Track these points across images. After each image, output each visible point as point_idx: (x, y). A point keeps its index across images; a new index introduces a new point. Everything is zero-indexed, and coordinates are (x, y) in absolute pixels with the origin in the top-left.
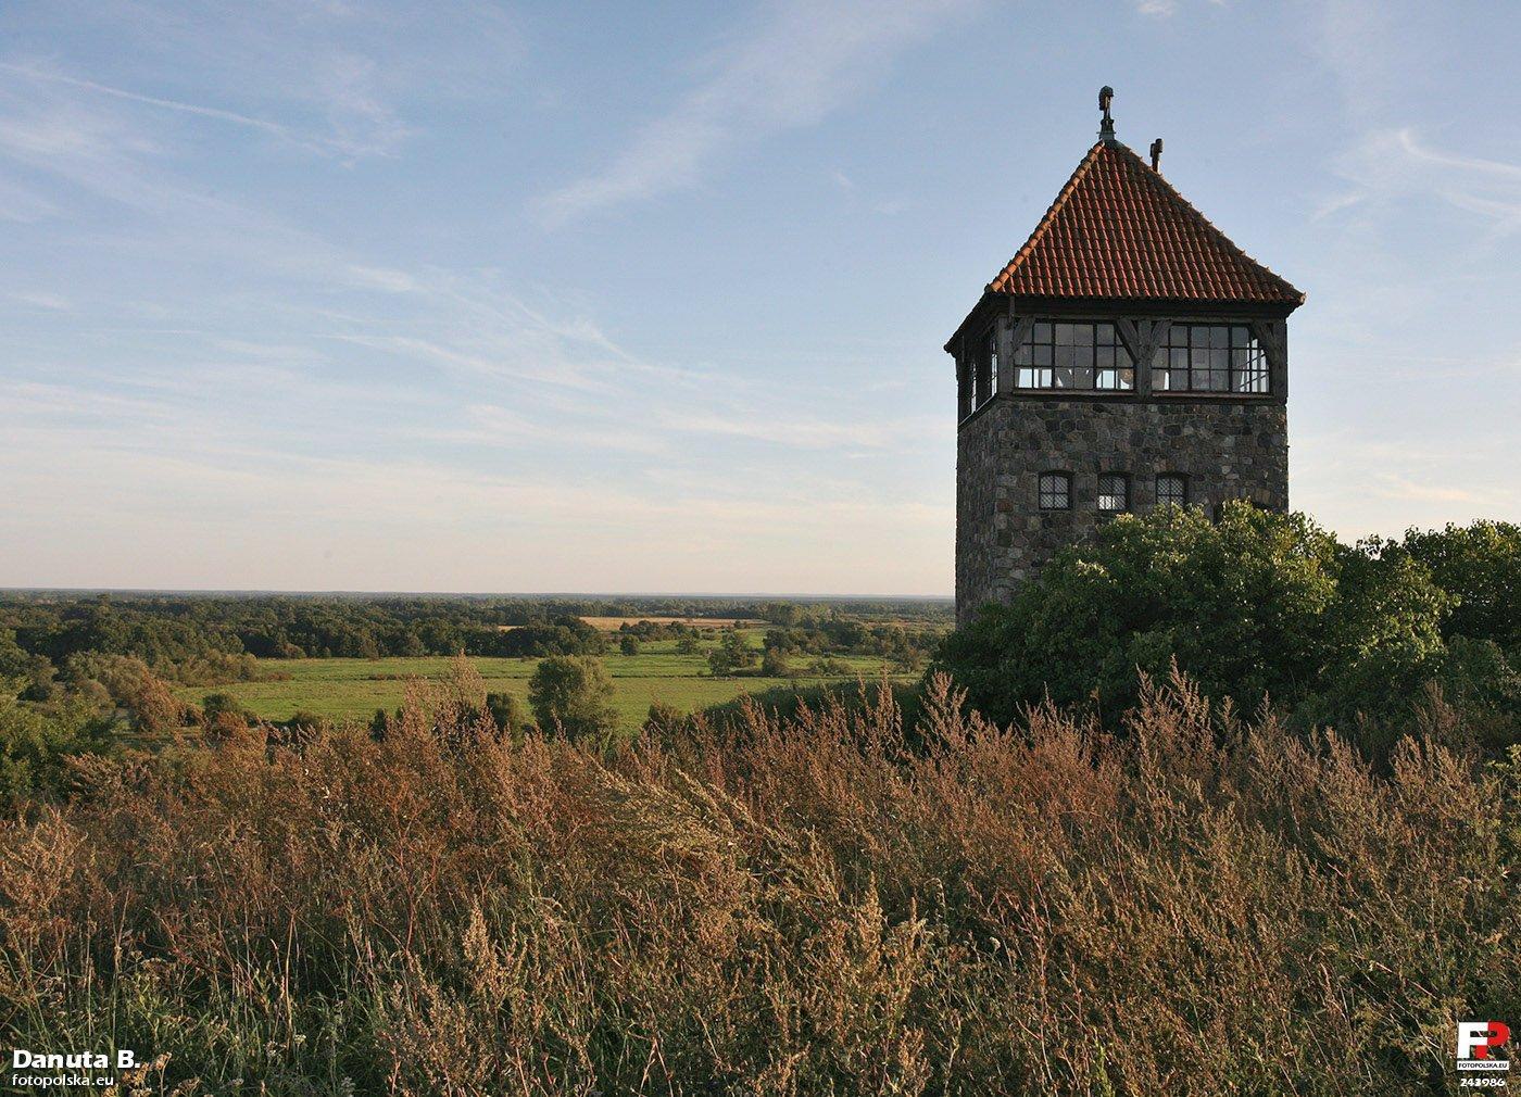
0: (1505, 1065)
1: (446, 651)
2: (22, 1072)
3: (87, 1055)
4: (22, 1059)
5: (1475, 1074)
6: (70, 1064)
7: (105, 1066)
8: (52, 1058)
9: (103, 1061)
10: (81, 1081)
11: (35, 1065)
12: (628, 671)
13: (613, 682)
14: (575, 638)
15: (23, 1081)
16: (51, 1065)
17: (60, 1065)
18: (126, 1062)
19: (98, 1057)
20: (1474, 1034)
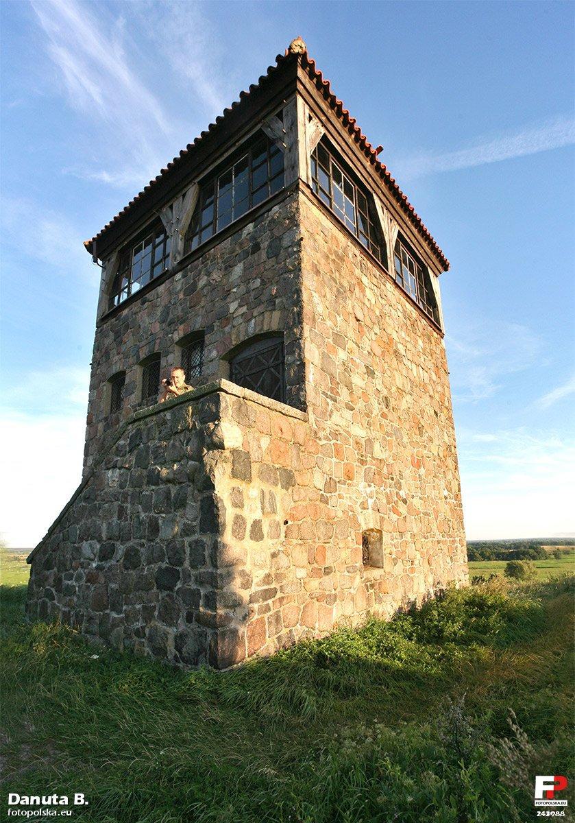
0: (564, 803)
1: (489, 559)
2: (14, 807)
3: (55, 797)
4: (14, 799)
5: (546, 809)
6: (44, 802)
7: (66, 803)
8: (33, 798)
9: (65, 800)
10: (51, 813)
11: (22, 803)
12: (557, 565)
13: (537, 570)
14: (535, 554)
15: (14, 813)
16: (32, 803)
17: (38, 803)
18: (79, 801)
19: (62, 797)
20: (546, 783)
